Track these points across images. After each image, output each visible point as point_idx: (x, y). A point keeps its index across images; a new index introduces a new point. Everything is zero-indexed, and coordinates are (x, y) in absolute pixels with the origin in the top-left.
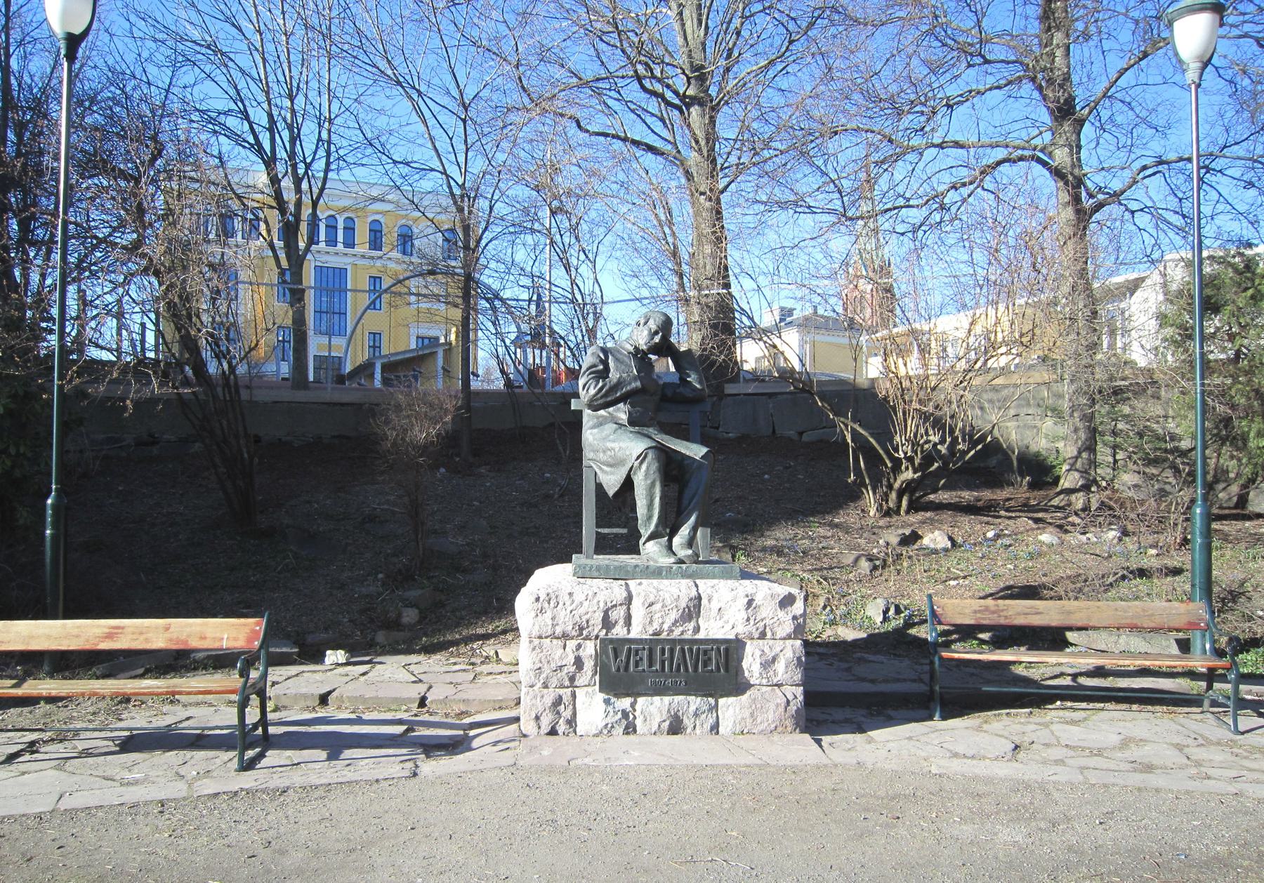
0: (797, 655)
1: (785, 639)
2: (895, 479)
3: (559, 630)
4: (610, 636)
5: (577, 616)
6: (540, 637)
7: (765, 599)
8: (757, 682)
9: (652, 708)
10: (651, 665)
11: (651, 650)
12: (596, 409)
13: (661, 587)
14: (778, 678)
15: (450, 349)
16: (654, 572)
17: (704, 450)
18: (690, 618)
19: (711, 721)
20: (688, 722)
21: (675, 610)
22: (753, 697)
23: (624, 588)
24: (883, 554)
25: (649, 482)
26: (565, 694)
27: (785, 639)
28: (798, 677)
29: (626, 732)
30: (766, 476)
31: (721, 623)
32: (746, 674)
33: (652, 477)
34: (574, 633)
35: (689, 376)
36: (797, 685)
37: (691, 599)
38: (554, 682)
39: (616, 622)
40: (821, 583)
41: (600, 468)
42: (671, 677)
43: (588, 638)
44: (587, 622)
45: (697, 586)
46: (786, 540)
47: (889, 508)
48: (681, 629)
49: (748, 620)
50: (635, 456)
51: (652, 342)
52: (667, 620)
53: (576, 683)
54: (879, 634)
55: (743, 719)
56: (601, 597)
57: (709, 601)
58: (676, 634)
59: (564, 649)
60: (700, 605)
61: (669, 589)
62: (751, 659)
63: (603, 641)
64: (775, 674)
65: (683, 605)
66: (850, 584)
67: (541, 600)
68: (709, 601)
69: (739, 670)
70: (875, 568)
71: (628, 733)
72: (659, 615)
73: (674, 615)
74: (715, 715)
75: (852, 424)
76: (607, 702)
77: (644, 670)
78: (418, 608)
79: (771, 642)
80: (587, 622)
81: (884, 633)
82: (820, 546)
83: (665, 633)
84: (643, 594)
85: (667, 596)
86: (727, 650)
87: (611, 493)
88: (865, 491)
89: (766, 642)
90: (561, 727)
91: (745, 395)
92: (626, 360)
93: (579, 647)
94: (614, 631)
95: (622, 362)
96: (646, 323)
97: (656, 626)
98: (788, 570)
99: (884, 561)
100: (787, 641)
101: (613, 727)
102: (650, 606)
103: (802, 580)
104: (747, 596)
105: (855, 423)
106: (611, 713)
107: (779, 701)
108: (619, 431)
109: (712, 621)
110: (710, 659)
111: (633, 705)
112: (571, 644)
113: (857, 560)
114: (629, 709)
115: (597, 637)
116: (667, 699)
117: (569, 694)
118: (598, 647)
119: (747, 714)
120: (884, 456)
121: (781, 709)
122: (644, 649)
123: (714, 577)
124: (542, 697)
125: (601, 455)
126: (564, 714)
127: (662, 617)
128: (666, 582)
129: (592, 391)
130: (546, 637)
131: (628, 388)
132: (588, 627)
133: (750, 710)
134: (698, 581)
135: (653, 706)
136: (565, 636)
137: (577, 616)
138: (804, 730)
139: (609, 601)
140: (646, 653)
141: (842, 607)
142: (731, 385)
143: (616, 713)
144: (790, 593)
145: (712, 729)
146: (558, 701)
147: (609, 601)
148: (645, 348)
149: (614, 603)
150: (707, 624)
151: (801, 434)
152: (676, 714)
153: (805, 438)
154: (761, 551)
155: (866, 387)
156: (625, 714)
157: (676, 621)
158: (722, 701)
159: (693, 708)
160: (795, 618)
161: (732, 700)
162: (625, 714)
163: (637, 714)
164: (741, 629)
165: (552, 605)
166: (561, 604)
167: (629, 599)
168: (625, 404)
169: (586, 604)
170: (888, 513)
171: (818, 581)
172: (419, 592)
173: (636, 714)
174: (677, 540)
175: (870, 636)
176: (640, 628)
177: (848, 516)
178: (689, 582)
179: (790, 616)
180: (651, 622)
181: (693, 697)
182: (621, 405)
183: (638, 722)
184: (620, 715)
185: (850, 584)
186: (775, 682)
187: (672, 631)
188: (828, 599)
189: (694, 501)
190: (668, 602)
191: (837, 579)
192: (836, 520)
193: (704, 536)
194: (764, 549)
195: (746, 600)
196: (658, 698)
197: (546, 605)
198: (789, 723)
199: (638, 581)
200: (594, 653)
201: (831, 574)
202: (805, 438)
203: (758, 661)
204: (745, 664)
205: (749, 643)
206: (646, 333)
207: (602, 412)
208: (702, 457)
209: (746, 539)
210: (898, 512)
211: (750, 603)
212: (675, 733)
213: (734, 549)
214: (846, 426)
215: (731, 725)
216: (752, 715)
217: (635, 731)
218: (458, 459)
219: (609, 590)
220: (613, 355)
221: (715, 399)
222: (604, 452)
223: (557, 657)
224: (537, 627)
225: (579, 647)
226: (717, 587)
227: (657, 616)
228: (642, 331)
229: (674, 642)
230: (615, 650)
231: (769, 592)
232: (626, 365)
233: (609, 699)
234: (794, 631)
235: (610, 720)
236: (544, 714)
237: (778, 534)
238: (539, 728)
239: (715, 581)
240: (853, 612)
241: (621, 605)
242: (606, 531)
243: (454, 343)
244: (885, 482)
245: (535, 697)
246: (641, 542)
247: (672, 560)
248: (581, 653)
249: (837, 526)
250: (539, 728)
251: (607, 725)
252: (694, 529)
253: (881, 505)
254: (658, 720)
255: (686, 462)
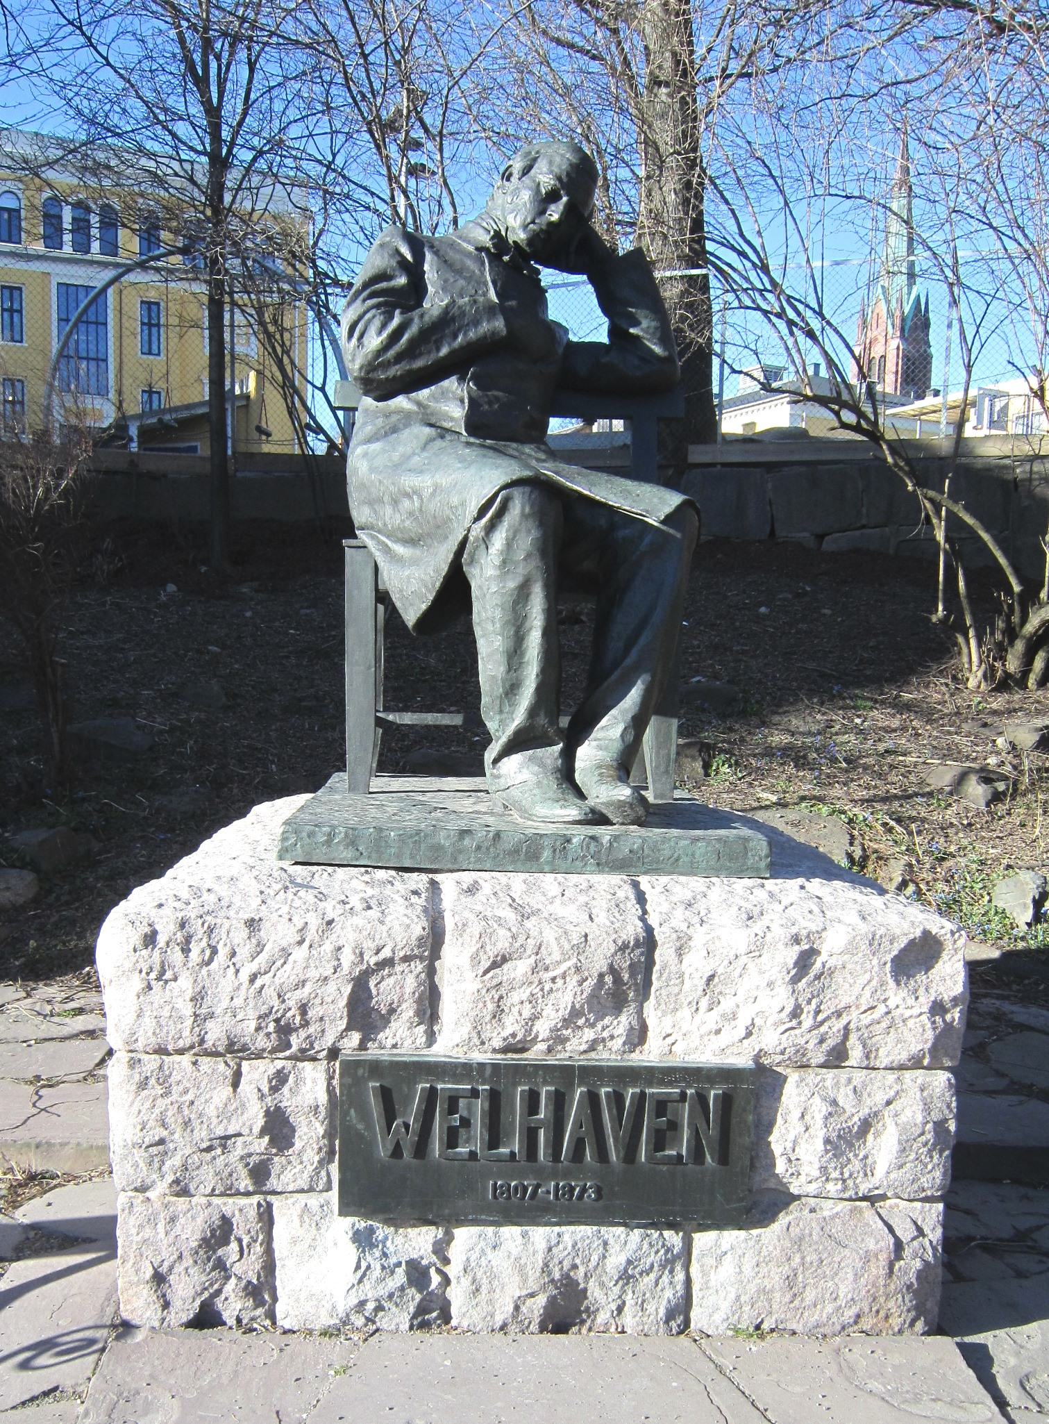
0: (935, 1116)
1: (902, 1067)
2: (1024, 619)
3: (215, 1034)
4: (373, 1052)
5: (270, 993)
6: (161, 1051)
7: (852, 948)
8: (812, 1189)
9: (497, 1259)
10: (494, 1143)
11: (495, 1098)
12: (384, 391)
13: (535, 901)
14: (875, 1181)
15: (247, 406)
16: (516, 851)
17: (672, 500)
18: (617, 1002)
19: (669, 1294)
20: (600, 1296)
21: (573, 981)
22: (795, 1231)
23: (420, 901)
24: (1009, 768)
25: (512, 584)
26: (243, 1210)
27: (902, 1067)
28: (934, 1175)
29: (421, 1322)
30: (763, 610)
31: (712, 1019)
32: (780, 1167)
33: (521, 571)
34: (261, 1042)
35: (636, 323)
36: (927, 1200)
37: (624, 948)
38: (206, 1178)
39: (392, 1011)
40: (890, 830)
41: (387, 550)
42: (555, 1175)
43: (304, 1055)
44: (303, 1009)
45: (641, 898)
46: (810, 734)
47: (1007, 675)
48: (589, 1034)
49: (796, 1013)
50: (473, 508)
51: (542, 221)
52: (548, 1011)
53: (273, 1183)
54: (1027, 952)
55: (762, 1291)
56: (348, 934)
57: (680, 952)
58: (575, 1048)
59: (235, 1085)
60: (650, 963)
61: (558, 909)
62: (796, 1127)
63: (350, 1068)
64: (867, 1171)
65: (601, 965)
66: (951, 831)
67: (161, 940)
68: (680, 952)
69: (760, 1155)
70: (997, 797)
71: (425, 1325)
72: (524, 994)
73: (568, 996)
74: (680, 1276)
75: (950, 504)
76: (363, 1240)
77: (473, 1155)
78: (36, 869)
79: (859, 1077)
80: (303, 1009)
81: (1038, 951)
82: (881, 747)
83: (542, 1047)
84: (475, 928)
85: (550, 935)
86: (726, 1101)
87: (411, 617)
88: (961, 639)
89: (843, 1075)
90: (232, 1305)
91: (724, 465)
92: (471, 265)
93: (280, 1079)
94: (387, 1036)
95: (459, 271)
96: (526, 170)
97: (511, 1026)
98: (821, 799)
99: (1015, 783)
100: (908, 1075)
101: (379, 1308)
102: (495, 965)
103: (851, 821)
104: (796, 940)
105: (956, 502)
106: (377, 1272)
107: (871, 1245)
108: (439, 443)
109: (686, 1012)
110: (674, 1126)
111: (440, 1249)
112: (256, 1073)
113: (962, 778)
114: (429, 1258)
115: (334, 1053)
116: (540, 1235)
117: (252, 1213)
118: (335, 1082)
119: (775, 1278)
120: (1009, 571)
121: (878, 1269)
122: (475, 1093)
123: (691, 870)
124: (173, 1220)
125: (388, 510)
126: (238, 1269)
127: (532, 999)
128: (550, 882)
129: (374, 341)
130: (181, 1052)
131: (472, 335)
132: (305, 1024)
133: (786, 1270)
134: (644, 881)
135: (500, 1253)
136: (236, 1050)
137: (270, 993)
138: (937, 1329)
139: (369, 945)
140: (480, 1105)
141: (940, 886)
142: (700, 448)
143: (390, 1271)
144: (926, 934)
145: (670, 1316)
146: (221, 1233)
147: (369, 945)
148: (521, 236)
149: (386, 953)
150: (668, 1021)
151: (820, 537)
152: (566, 1276)
153: (828, 545)
154: (763, 755)
155: (943, 454)
156: (417, 1274)
157: (575, 1013)
158: (703, 1240)
159: (616, 1260)
160: (938, 1008)
161: (731, 1237)
162: (417, 1274)
163: (452, 1271)
164: (770, 1040)
165: (195, 955)
166: (223, 952)
167: (434, 940)
168: (462, 379)
169: (300, 954)
170: (1004, 684)
171: (885, 824)
172: (43, 834)
173: (452, 1271)
174: (587, 754)
175: (1008, 956)
176: (465, 1030)
177: (936, 692)
178: (610, 884)
179: (925, 1003)
180: (498, 1013)
181: (620, 1230)
182: (451, 383)
183: (457, 1295)
184: (400, 1277)
185: (951, 831)
186: (863, 1189)
187: (563, 1041)
188: (910, 865)
189: (642, 641)
190: (553, 953)
191: (923, 820)
192: (906, 696)
193: (661, 743)
194: (769, 752)
195: (793, 953)
196: (516, 1230)
197: (176, 956)
198: (898, 1308)
199: (467, 878)
200: (323, 1098)
201: (908, 810)
202: (828, 545)
203: (819, 1134)
204: (778, 1141)
205: (793, 1077)
206: (526, 195)
207: (401, 402)
208: (667, 520)
209: (731, 730)
210: (1022, 683)
211: (805, 961)
212: (561, 1328)
213: (707, 753)
214: (937, 507)
215: (725, 1306)
216: (790, 1281)
217: (446, 1317)
218: (203, 569)
219: (374, 914)
220: (436, 253)
221: (670, 472)
222: (395, 502)
223: (211, 1111)
224: (148, 1023)
225: (280, 1079)
226: (701, 906)
227: (515, 997)
228: (516, 192)
229: (566, 1075)
230: (386, 1095)
231: (863, 928)
232: (469, 280)
233: (371, 1230)
234: (934, 1050)
235: (370, 1291)
236: (179, 1268)
237: (795, 722)
238: (166, 1305)
239: (696, 883)
240: (965, 898)
241: (406, 959)
242: (407, 718)
243: (253, 394)
244: (1000, 624)
245: (152, 1220)
246: (490, 754)
247: (573, 812)
248: (287, 1099)
249: (908, 707)
250: (166, 1305)
251: (362, 1304)
252: (638, 724)
253: (992, 668)
254: (514, 1290)
255: (621, 534)
